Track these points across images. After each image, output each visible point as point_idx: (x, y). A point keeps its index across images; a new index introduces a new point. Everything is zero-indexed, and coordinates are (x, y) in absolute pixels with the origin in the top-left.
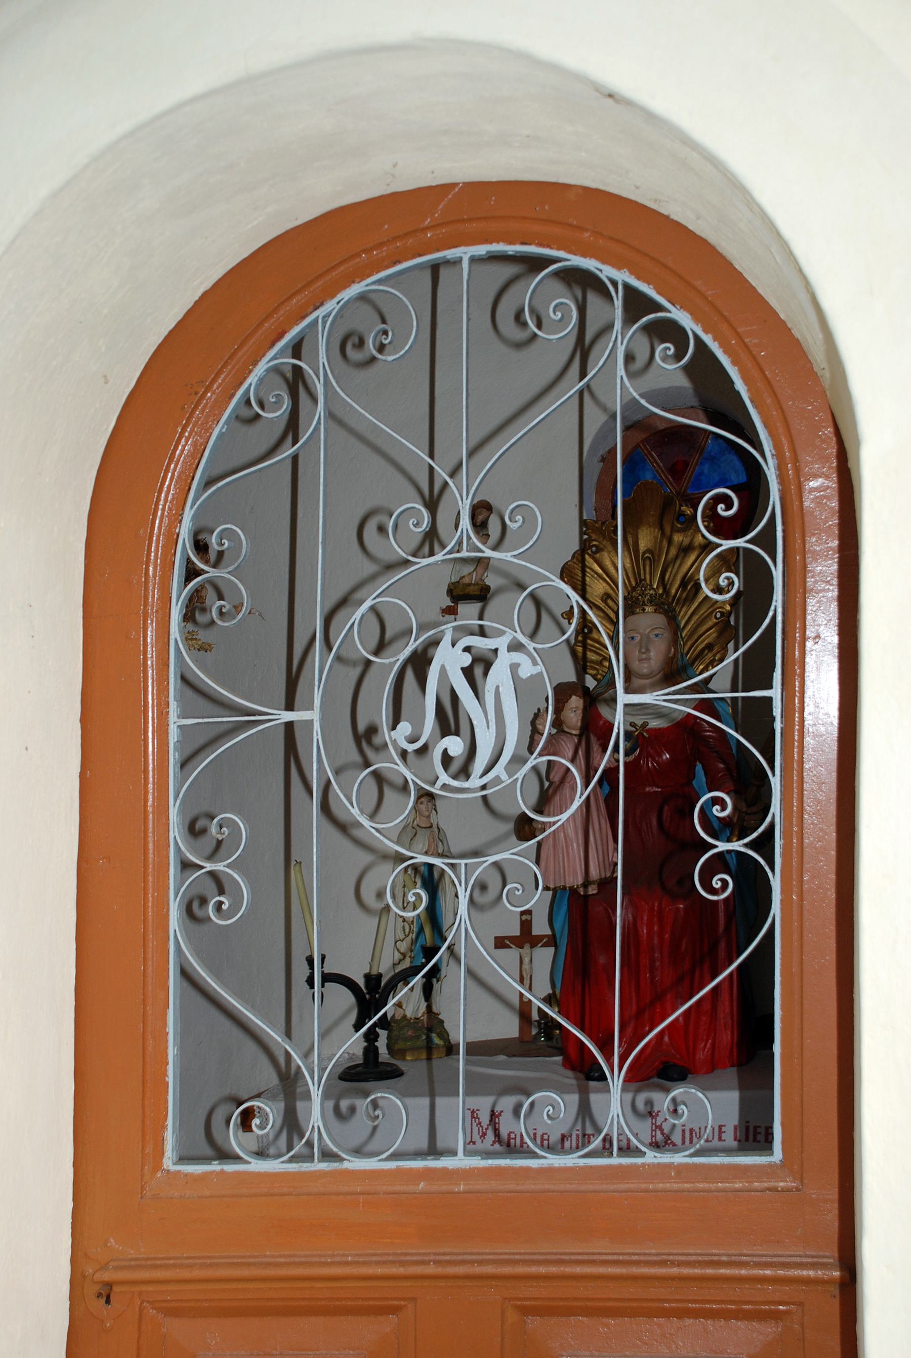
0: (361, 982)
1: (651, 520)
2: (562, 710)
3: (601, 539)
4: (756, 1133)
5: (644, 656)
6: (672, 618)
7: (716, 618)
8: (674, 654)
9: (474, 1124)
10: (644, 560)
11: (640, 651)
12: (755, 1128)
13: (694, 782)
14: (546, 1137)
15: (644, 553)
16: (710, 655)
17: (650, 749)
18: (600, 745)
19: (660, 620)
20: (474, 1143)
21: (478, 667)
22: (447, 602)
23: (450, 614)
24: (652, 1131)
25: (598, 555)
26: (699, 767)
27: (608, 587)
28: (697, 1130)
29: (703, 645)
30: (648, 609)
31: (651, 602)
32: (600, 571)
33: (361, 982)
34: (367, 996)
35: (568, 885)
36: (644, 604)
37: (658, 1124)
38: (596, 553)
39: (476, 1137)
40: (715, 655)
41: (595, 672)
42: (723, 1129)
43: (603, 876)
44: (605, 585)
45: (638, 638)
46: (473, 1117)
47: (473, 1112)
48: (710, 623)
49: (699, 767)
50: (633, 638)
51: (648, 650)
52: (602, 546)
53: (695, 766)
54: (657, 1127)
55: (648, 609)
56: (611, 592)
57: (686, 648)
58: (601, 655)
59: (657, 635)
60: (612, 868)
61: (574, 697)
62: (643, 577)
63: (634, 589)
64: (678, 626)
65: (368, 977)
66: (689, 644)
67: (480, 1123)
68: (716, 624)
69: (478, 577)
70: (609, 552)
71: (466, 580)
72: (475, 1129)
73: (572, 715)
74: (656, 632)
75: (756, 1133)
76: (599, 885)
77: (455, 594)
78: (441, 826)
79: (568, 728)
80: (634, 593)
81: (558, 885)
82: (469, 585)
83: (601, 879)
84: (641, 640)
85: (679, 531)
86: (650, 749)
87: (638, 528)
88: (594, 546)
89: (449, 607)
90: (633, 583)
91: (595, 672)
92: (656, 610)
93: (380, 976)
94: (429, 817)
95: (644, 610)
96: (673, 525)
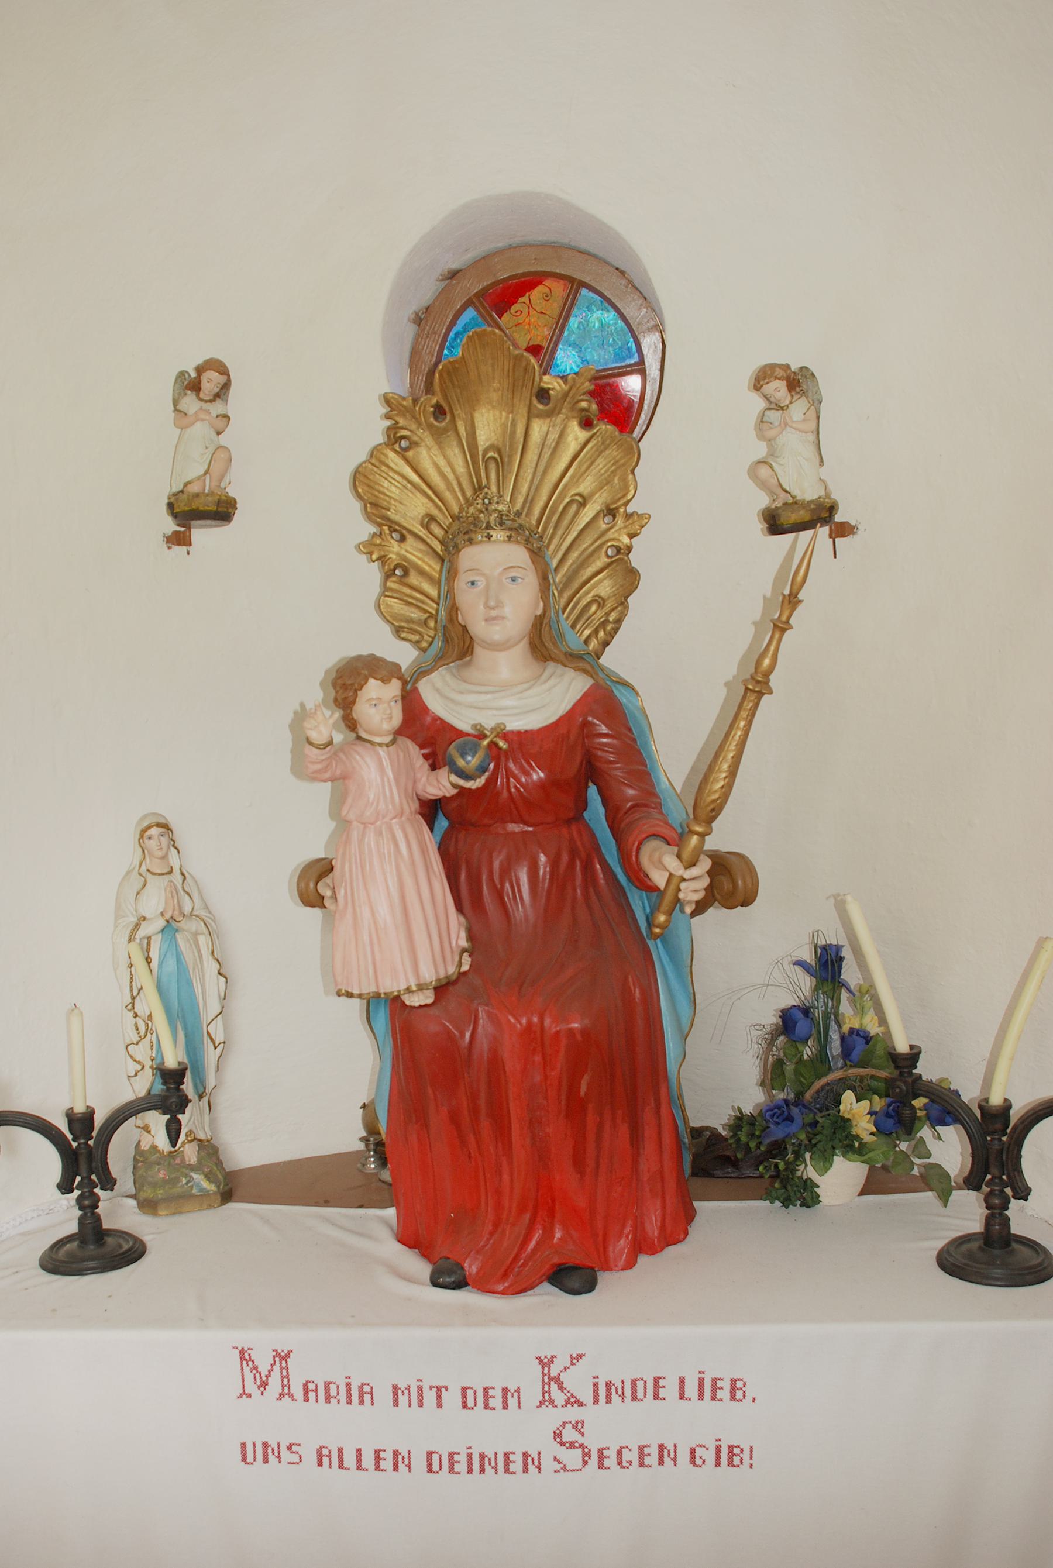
0: (63, 1126)
1: (495, 396)
2: (354, 702)
3: (414, 427)
4: (714, 1388)
5: (493, 613)
6: (537, 554)
7: (608, 556)
8: (545, 611)
9: (247, 1370)
10: (486, 462)
11: (486, 606)
12: (714, 1381)
13: (585, 814)
14: (366, 1389)
15: (486, 452)
16: (600, 614)
17: (511, 765)
18: (426, 757)
19: (519, 555)
20: (249, 1396)
21: (586, 642)
22: (171, 526)
23: (179, 544)
24: (544, 1383)
25: (410, 454)
26: (593, 791)
27: (430, 505)
28: (615, 1397)
29: (589, 598)
30: (498, 535)
31: (501, 524)
32: (415, 478)
33: (63, 1126)
34: (74, 1144)
35: (382, 991)
36: (489, 527)
37: (554, 1374)
38: (406, 450)
39: (251, 1387)
40: (608, 614)
41: (417, 638)
42: (661, 1382)
43: (442, 975)
44: (425, 500)
45: (481, 584)
46: (242, 1358)
47: (242, 1352)
48: (599, 564)
49: (593, 791)
50: (473, 583)
51: (499, 605)
52: (415, 438)
53: (587, 787)
54: (550, 1379)
55: (498, 535)
56: (435, 512)
57: (563, 602)
58: (426, 611)
59: (513, 579)
60: (457, 959)
61: (372, 681)
62: (484, 482)
63: (469, 504)
64: (547, 565)
65: (71, 1117)
66: (566, 595)
67: (256, 1368)
68: (609, 565)
69: (214, 483)
70: (429, 449)
71: (194, 488)
72: (249, 1377)
73: (373, 711)
74: (513, 573)
75: (714, 1388)
76: (436, 989)
77: (177, 510)
78: (188, 869)
79: (366, 731)
80: (471, 510)
81: (364, 991)
82: (197, 495)
83: (438, 980)
84: (487, 588)
85: (541, 415)
86: (511, 765)
87: (473, 409)
88: (403, 437)
89: (176, 533)
90: (469, 493)
91: (417, 638)
92: (509, 537)
93: (90, 1114)
94: (165, 857)
95: (489, 537)
96: (530, 406)
